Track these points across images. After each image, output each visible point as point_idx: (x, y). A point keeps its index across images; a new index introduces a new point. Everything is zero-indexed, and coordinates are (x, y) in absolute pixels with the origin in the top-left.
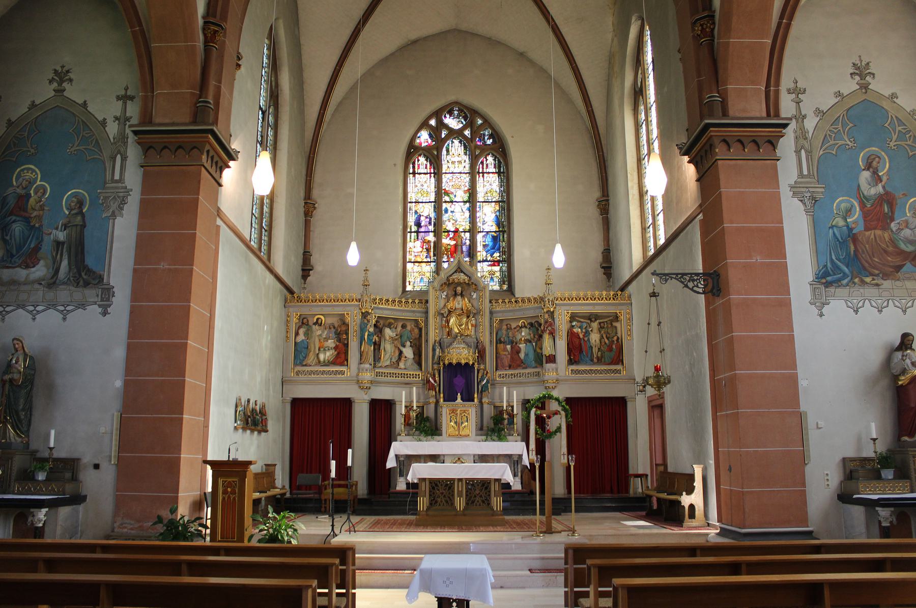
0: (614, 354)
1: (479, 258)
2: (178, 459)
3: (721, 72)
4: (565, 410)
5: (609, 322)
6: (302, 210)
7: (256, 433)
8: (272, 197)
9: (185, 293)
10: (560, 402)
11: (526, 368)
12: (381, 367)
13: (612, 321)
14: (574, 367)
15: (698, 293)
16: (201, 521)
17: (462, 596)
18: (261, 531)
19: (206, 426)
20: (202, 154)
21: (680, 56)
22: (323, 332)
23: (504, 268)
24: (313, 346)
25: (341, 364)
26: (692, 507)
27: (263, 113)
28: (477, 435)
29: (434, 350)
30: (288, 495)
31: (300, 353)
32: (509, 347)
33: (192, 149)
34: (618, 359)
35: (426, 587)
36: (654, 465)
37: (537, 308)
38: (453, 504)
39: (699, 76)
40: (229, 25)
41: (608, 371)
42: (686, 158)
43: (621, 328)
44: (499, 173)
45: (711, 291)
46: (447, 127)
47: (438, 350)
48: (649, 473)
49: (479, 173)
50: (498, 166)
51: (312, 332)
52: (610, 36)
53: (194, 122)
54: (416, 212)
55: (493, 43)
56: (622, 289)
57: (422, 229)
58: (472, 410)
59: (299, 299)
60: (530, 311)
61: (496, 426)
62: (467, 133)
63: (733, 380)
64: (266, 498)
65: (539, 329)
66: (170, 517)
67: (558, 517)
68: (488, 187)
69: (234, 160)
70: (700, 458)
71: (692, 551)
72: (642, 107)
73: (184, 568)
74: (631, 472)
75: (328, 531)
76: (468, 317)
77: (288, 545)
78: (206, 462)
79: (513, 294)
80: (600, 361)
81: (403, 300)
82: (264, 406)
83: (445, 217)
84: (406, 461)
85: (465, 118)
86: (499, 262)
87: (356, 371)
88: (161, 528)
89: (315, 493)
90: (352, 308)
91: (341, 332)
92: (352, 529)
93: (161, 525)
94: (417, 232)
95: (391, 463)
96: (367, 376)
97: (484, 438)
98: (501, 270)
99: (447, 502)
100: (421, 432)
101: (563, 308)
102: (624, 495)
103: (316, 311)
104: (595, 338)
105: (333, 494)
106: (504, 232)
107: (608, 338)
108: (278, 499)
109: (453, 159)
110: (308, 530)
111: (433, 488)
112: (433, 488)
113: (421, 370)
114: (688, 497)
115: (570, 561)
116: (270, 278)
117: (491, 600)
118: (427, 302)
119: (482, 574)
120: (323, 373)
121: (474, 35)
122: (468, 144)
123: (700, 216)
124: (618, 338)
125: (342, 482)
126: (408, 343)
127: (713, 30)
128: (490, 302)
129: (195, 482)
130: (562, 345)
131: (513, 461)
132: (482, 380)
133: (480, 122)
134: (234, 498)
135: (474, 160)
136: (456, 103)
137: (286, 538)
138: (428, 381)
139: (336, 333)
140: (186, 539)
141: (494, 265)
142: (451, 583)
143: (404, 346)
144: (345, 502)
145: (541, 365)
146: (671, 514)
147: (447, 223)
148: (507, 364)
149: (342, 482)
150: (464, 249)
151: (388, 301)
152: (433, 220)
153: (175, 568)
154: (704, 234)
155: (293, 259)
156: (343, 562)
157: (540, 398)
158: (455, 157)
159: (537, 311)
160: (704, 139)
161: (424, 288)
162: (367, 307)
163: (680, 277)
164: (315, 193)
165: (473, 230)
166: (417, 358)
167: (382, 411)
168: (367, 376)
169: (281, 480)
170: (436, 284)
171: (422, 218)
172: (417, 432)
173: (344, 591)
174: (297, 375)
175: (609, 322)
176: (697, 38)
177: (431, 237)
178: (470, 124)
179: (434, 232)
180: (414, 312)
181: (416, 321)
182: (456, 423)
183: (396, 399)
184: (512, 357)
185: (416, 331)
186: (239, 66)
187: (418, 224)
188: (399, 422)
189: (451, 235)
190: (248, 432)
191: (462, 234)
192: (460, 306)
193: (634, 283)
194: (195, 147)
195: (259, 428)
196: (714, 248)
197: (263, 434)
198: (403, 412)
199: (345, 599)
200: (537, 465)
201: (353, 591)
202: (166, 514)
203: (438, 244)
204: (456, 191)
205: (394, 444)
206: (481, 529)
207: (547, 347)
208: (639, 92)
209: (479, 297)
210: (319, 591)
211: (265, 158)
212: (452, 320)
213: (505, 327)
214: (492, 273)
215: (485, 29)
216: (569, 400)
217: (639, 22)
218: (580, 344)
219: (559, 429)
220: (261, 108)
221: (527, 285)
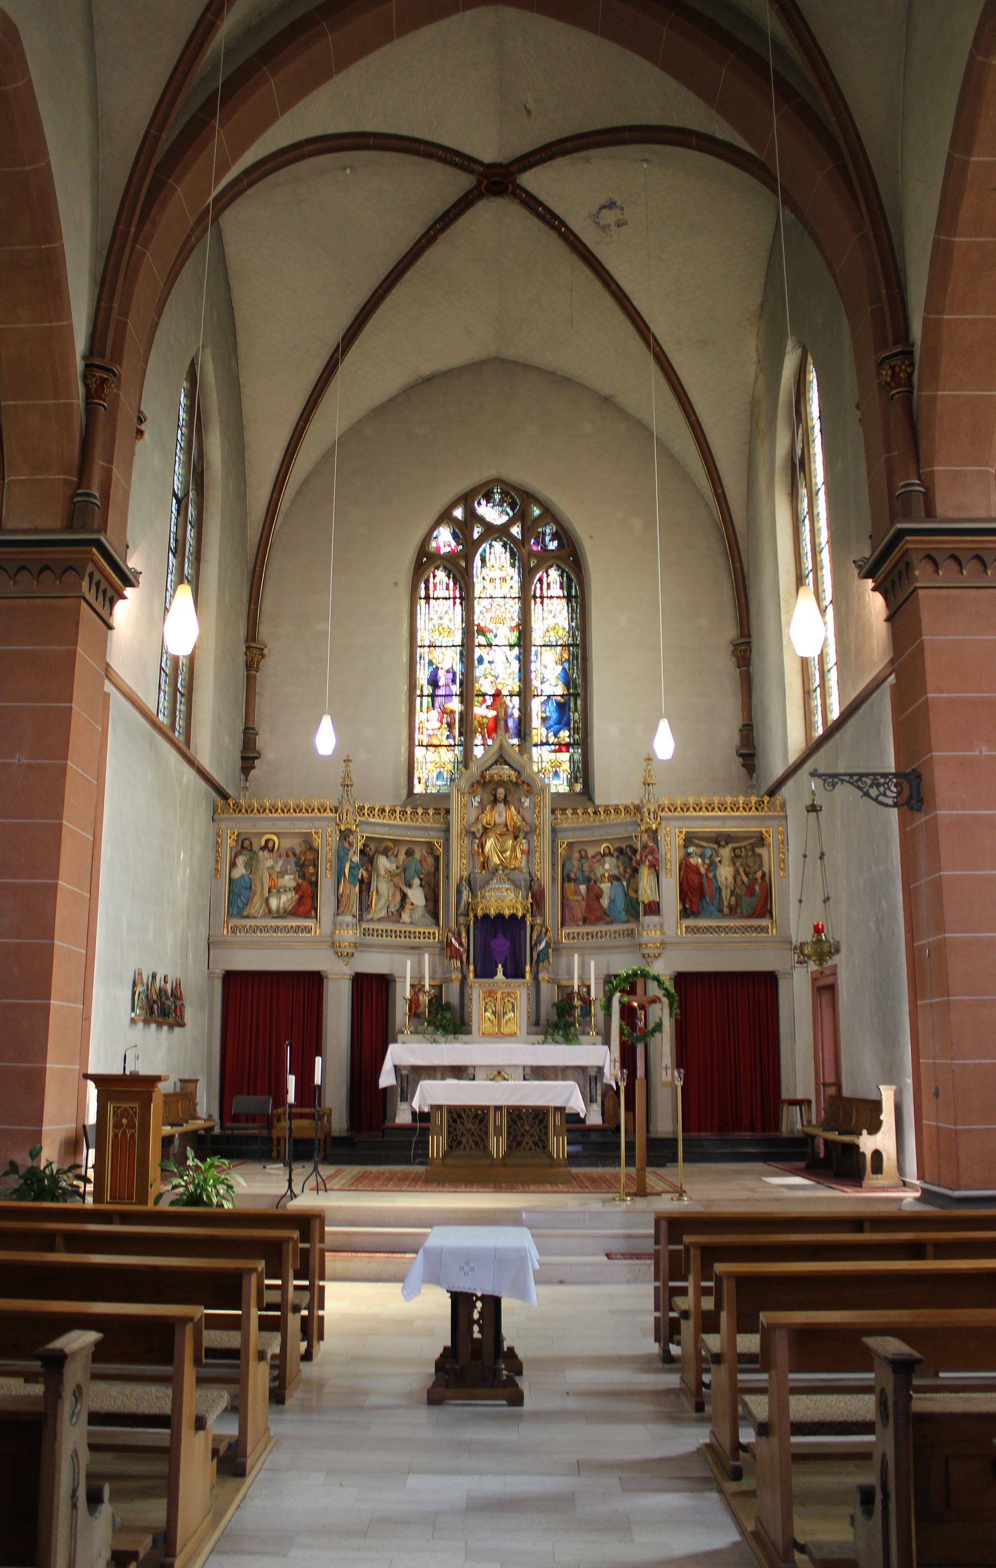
0: (757, 901)
1: (536, 739)
2: (42, 1072)
3: (923, 445)
4: (668, 995)
5: (748, 848)
6: (242, 660)
7: (165, 1028)
8: (192, 658)
9: (53, 801)
10: (660, 983)
11: (611, 923)
12: (371, 920)
13: (753, 846)
14: (691, 922)
15: (886, 805)
16: (77, 1171)
17: (489, 1290)
18: (175, 1187)
19: (86, 1018)
20: (83, 579)
21: (858, 414)
22: (276, 862)
23: (576, 757)
24: (258, 885)
25: (306, 915)
26: (877, 1155)
27: (178, 502)
28: (529, 1033)
29: (459, 892)
30: (217, 1130)
31: (239, 898)
32: (583, 888)
33: (66, 571)
34: (764, 909)
35: (433, 1278)
36: (820, 1084)
37: (629, 824)
38: (486, 1147)
39: (888, 449)
40: (125, 369)
41: (745, 929)
42: (870, 583)
43: (769, 856)
44: (569, 598)
45: (908, 803)
46: (481, 521)
47: (465, 893)
48: (812, 1097)
49: (535, 597)
50: (567, 585)
51: (258, 861)
52: (752, 370)
53: (69, 528)
54: (431, 663)
55: (560, 381)
56: (772, 792)
57: (441, 692)
58: (521, 992)
59: (238, 808)
60: (618, 828)
61: (561, 1020)
62: (516, 530)
63: (941, 947)
64: (183, 1135)
65: (633, 857)
66: (30, 1163)
67: (661, 1171)
68: (550, 622)
69: (132, 585)
70: (890, 1077)
71: (856, 1223)
72: (804, 491)
73: (59, 1241)
74: (785, 1095)
75: (282, 1189)
76: (516, 838)
77: (219, 1210)
78: (87, 1076)
79: (591, 799)
80: (733, 911)
81: (409, 810)
82: (178, 984)
83: (479, 671)
84: (411, 1076)
85: (513, 506)
86: (567, 746)
87: (330, 927)
88: (14, 1182)
89: (263, 1128)
90: (324, 824)
91: (305, 863)
92: (321, 1186)
93: (16, 1177)
94: (433, 696)
95: (387, 1079)
96: (349, 935)
97: (541, 1038)
98: (571, 760)
99: (476, 1143)
100: (437, 1028)
101: (673, 823)
102: (773, 1134)
103: (267, 828)
104: (725, 873)
105: (290, 1129)
106: (576, 696)
107: (747, 874)
108: (201, 1136)
109: (492, 575)
110: (250, 1186)
111: (455, 1121)
112: (455, 1121)
113: (438, 925)
114: (872, 1138)
115: (663, 1238)
116: (189, 774)
117: (534, 1297)
118: (448, 812)
119: (520, 1257)
120: (276, 929)
121: (527, 367)
122: (517, 551)
123: (892, 679)
124: (764, 875)
125: (306, 1110)
126: (416, 882)
127: (910, 376)
128: (553, 812)
129: (71, 1107)
130: (670, 892)
131: (588, 1077)
132: (539, 941)
133: (537, 512)
134: (132, 1135)
135: (526, 577)
136: (498, 481)
137: (215, 1200)
138: (449, 944)
139: (297, 864)
140: (54, 1198)
141: (560, 751)
142: (472, 1269)
143: (410, 886)
144: (310, 1142)
145: (637, 918)
146: (845, 1166)
147: (482, 681)
148: (580, 916)
149: (306, 1110)
150: (511, 724)
151: (383, 811)
152: (458, 676)
153: (47, 1241)
154: (898, 709)
155: (227, 740)
156: (305, 1237)
157: (628, 976)
158: (496, 571)
159: (630, 828)
160: (896, 554)
161: (444, 790)
162: (349, 822)
163: (856, 779)
164: (264, 631)
165: (525, 693)
166: (431, 906)
167: (372, 992)
168: (349, 935)
169: (206, 1105)
170: (464, 784)
171: (441, 673)
172: (431, 1029)
173: (306, 1283)
174: (234, 932)
175: (748, 848)
176: (885, 387)
177: (455, 705)
178: (521, 516)
179: (461, 695)
180: (426, 829)
181: (430, 845)
182: (494, 1013)
183: (397, 973)
184: (587, 903)
185: (430, 860)
186: (140, 433)
187: (434, 682)
188: (401, 1010)
189: (489, 701)
190: (153, 1026)
191: (508, 699)
192: (502, 820)
193: (790, 784)
194: (70, 568)
195: (171, 1020)
196: (912, 732)
197: (177, 1030)
198: (408, 995)
199: (307, 1295)
200: (622, 1085)
201: (321, 1283)
202: (23, 1160)
203: (466, 717)
204: (495, 626)
205: (391, 1047)
206: (532, 1188)
207: (646, 888)
208: (798, 466)
209: (534, 805)
210: (267, 1282)
211: (184, 593)
212: (489, 844)
213: (576, 855)
214: (556, 765)
215: (546, 358)
216: (682, 979)
217: (799, 351)
218: (701, 884)
219: (658, 1027)
220: (175, 495)
221: (613, 787)
